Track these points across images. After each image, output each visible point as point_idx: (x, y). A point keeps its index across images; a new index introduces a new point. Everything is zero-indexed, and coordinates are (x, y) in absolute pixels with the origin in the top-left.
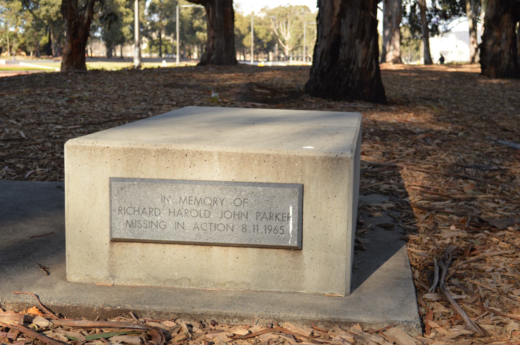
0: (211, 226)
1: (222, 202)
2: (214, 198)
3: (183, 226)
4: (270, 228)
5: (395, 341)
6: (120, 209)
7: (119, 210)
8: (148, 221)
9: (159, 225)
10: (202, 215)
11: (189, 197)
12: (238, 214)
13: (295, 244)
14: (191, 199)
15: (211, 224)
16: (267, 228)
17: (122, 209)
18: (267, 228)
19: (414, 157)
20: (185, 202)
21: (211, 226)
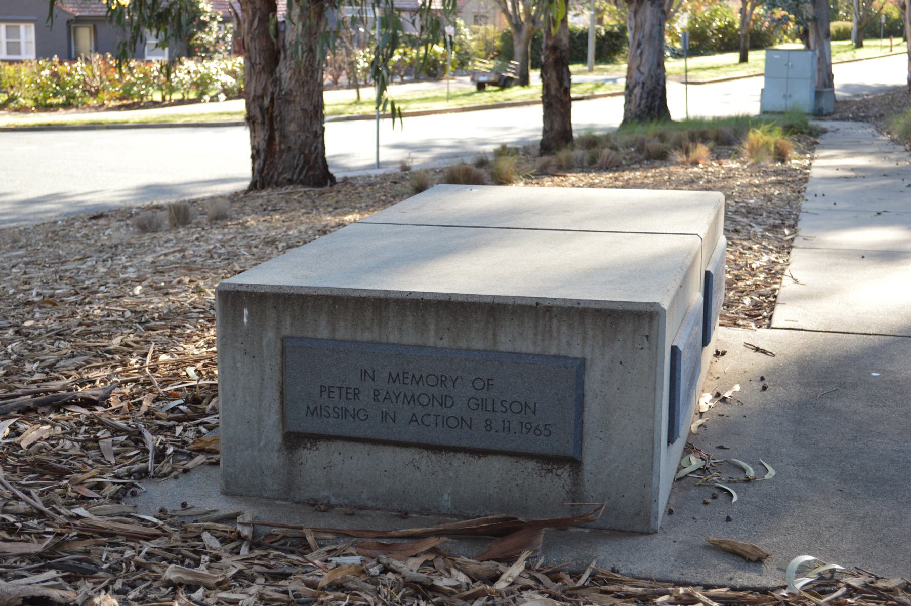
1: (454, 382)
4: (529, 426)
10: (490, 407)
14: (406, 375)
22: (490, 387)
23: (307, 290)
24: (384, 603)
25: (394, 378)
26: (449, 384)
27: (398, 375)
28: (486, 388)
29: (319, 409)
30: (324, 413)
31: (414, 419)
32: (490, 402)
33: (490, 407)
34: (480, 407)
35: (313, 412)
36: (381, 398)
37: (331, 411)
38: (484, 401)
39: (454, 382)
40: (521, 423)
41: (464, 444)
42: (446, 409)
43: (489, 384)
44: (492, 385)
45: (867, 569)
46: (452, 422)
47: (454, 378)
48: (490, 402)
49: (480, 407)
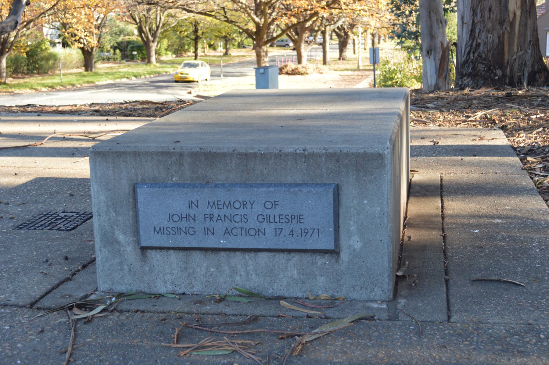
0: (241, 231)
1: (252, 205)
2: (243, 201)
3: (212, 231)
4: (306, 231)
5: (16, 176)
6: (245, 203)
7: (243, 205)
8: (176, 227)
9: (187, 231)
10: (272, 220)
11: (218, 201)
12: (183, 219)
13: (331, 246)
14: (219, 203)
15: (241, 228)
16: (303, 232)
17: (246, 203)
18: (303, 232)
19: (347, 176)
20: (214, 207)
21: (241, 231)
22: (276, 206)
23: (8, 153)
24: (1, 352)
25: (212, 205)
26: (249, 206)
27: (214, 203)
28: (242, 207)
29: (162, 230)
30: (165, 232)
31: (227, 232)
32: (272, 217)
33: (272, 220)
34: (266, 221)
35: (160, 231)
36: (215, 219)
37: (172, 232)
38: (268, 217)
39: (252, 205)
40: (301, 229)
41: (195, 245)
42: (301, 224)
43: (275, 205)
44: (278, 205)
45: (192, 324)
46: (252, 232)
47: (252, 202)
48: (272, 217)
49: (266, 221)
